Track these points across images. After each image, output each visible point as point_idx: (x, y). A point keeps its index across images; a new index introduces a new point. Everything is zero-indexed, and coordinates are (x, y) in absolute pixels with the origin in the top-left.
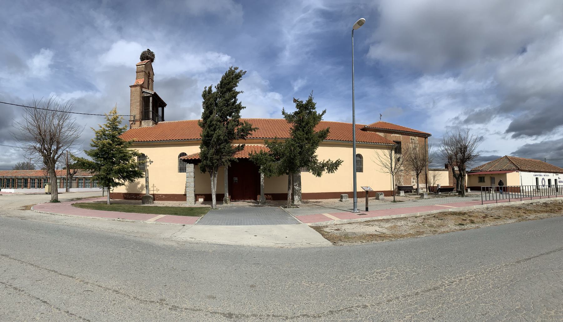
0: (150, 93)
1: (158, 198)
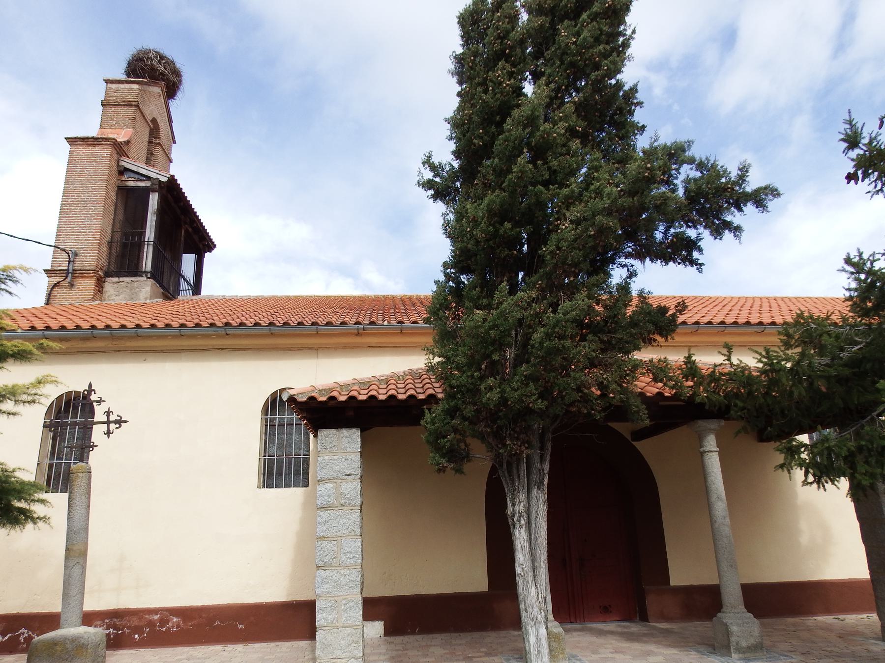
0: (153, 175)
1: (141, 633)
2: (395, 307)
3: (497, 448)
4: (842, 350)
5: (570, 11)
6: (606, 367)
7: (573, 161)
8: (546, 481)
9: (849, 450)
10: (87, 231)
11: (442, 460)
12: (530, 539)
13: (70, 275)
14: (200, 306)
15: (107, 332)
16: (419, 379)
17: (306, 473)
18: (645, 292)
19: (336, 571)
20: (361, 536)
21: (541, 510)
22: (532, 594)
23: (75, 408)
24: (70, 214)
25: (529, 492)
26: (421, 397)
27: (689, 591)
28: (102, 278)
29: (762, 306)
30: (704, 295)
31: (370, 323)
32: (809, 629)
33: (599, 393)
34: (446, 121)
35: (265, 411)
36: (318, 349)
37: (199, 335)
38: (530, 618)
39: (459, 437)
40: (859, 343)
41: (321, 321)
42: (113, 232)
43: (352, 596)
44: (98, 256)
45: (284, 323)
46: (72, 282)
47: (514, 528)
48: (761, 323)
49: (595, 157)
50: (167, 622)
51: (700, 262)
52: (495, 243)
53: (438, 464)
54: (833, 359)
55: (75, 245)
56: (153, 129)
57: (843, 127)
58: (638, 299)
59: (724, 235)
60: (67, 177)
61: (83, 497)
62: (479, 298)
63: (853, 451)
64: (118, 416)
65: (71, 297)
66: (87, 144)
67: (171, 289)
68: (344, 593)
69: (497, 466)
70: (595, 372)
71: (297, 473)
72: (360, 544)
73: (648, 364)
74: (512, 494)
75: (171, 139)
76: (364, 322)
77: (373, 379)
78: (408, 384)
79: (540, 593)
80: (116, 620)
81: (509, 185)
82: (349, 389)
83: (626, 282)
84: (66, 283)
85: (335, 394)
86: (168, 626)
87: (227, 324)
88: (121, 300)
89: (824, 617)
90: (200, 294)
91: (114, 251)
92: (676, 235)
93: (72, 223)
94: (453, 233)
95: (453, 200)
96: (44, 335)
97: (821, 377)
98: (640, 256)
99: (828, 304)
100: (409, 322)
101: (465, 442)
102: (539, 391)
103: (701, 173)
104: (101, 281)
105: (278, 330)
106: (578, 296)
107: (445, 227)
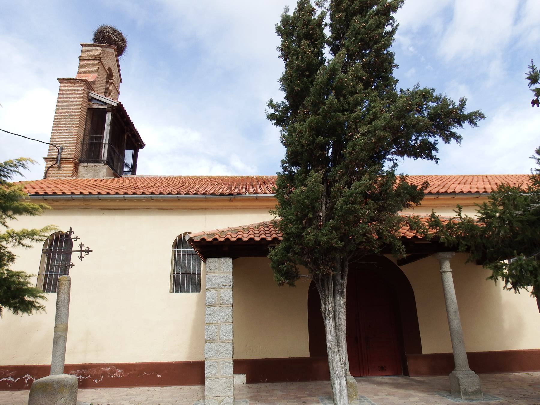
0: (109, 102)
2: (253, 184)
3: (314, 271)
4: (528, 206)
5: (356, 11)
6: (380, 221)
8: (345, 290)
9: (534, 266)
10: (70, 135)
11: (282, 278)
12: (335, 326)
13: (59, 161)
15: (81, 196)
16: (268, 228)
17: (199, 284)
20: (232, 323)
21: (342, 308)
22: (337, 359)
23: (61, 242)
24: (59, 125)
25: (335, 297)
26: (269, 239)
28: (77, 163)
29: (478, 181)
30: (447, 175)
31: (238, 194)
32: (510, 381)
35: (174, 246)
36: (206, 209)
38: (336, 374)
39: (291, 264)
41: (209, 192)
42: (84, 136)
43: (227, 359)
44: (75, 150)
45: (186, 193)
46: (60, 166)
47: (326, 319)
48: (477, 192)
49: (374, 94)
50: (115, 372)
51: (437, 157)
53: (279, 281)
54: (524, 211)
55: (62, 143)
56: (109, 74)
57: (528, 70)
59: (451, 141)
60: (58, 102)
64: (87, 247)
66: (70, 83)
67: (119, 170)
68: (222, 357)
71: (193, 284)
72: (232, 328)
73: (407, 219)
74: (324, 298)
75: (120, 80)
76: (234, 193)
77: (240, 228)
78: (260, 228)
79: (342, 358)
82: (226, 234)
83: (392, 170)
84: (56, 166)
85: (217, 237)
86: (115, 375)
87: (152, 193)
88: (89, 177)
89: (520, 373)
90: (135, 174)
91: (85, 147)
92: (422, 141)
93: (60, 130)
95: (287, 125)
96: (43, 198)
98: (401, 154)
99: (520, 179)
100: (261, 193)
101: (296, 267)
102: (339, 236)
103: (437, 103)
104: (77, 165)
105: (183, 197)
106: (363, 178)
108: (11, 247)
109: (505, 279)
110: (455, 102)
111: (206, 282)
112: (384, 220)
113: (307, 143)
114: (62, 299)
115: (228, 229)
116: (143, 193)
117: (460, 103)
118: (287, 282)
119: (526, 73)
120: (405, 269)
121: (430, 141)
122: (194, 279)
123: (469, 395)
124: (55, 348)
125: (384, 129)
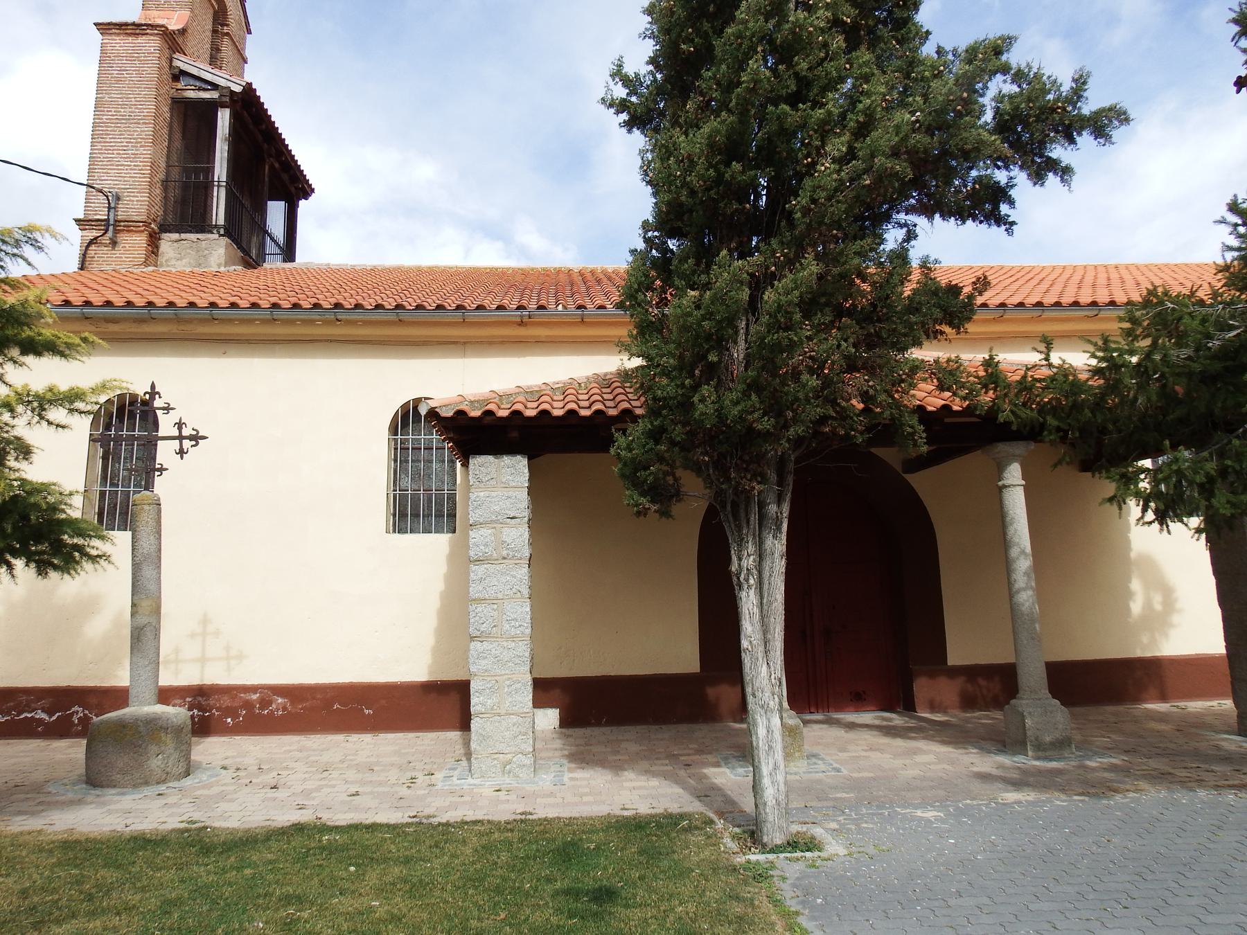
0: (222, 82)
1: (235, 715)
2: (572, 285)
3: (717, 482)
4: (1209, 337)
7: (832, 66)
9: (1207, 475)
11: (642, 500)
12: (761, 603)
13: (111, 228)
14: (295, 279)
15: (170, 311)
17: (452, 516)
18: (931, 259)
19: (497, 643)
22: (762, 675)
23: (132, 416)
26: (613, 412)
27: (972, 672)
28: (155, 233)
30: (1014, 265)
31: (538, 308)
33: (861, 406)
34: (611, 106)
35: (394, 429)
36: (465, 343)
37: (298, 320)
40: (1236, 328)
41: (470, 304)
42: (168, 166)
45: (417, 306)
50: (270, 703)
51: (1011, 219)
52: (717, 193)
53: (637, 505)
54: (1197, 350)
58: (919, 271)
61: (152, 538)
62: (694, 272)
63: (1212, 476)
65: (114, 259)
69: (718, 507)
70: (857, 378)
71: (439, 515)
72: (528, 609)
77: (544, 387)
80: (201, 699)
81: (737, 104)
85: (492, 407)
87: (337, 306)
92: (978, 180)
94: (658, 180)
96: (83, 313)
97: (1178, 375)
98: (927, 211)
103: (1019, 86)
104: (156, 238)
107: (645, 171)
108: (23, 427)
109: (1141, 503)
110: (1061, 84)
111: (468, 508)
112: (881, 367)
113: (702, 184)
114: (145, 545)
115: (517, 390)
116: (316, 306)
117: (1074, 86)
118: (654, 508)
119: (1230, 9)
120: (920, 482)
121: (998, 179)
122: (440, 503)
123: (1044, 750)
124: (135, 651)
125: (895, 153)
